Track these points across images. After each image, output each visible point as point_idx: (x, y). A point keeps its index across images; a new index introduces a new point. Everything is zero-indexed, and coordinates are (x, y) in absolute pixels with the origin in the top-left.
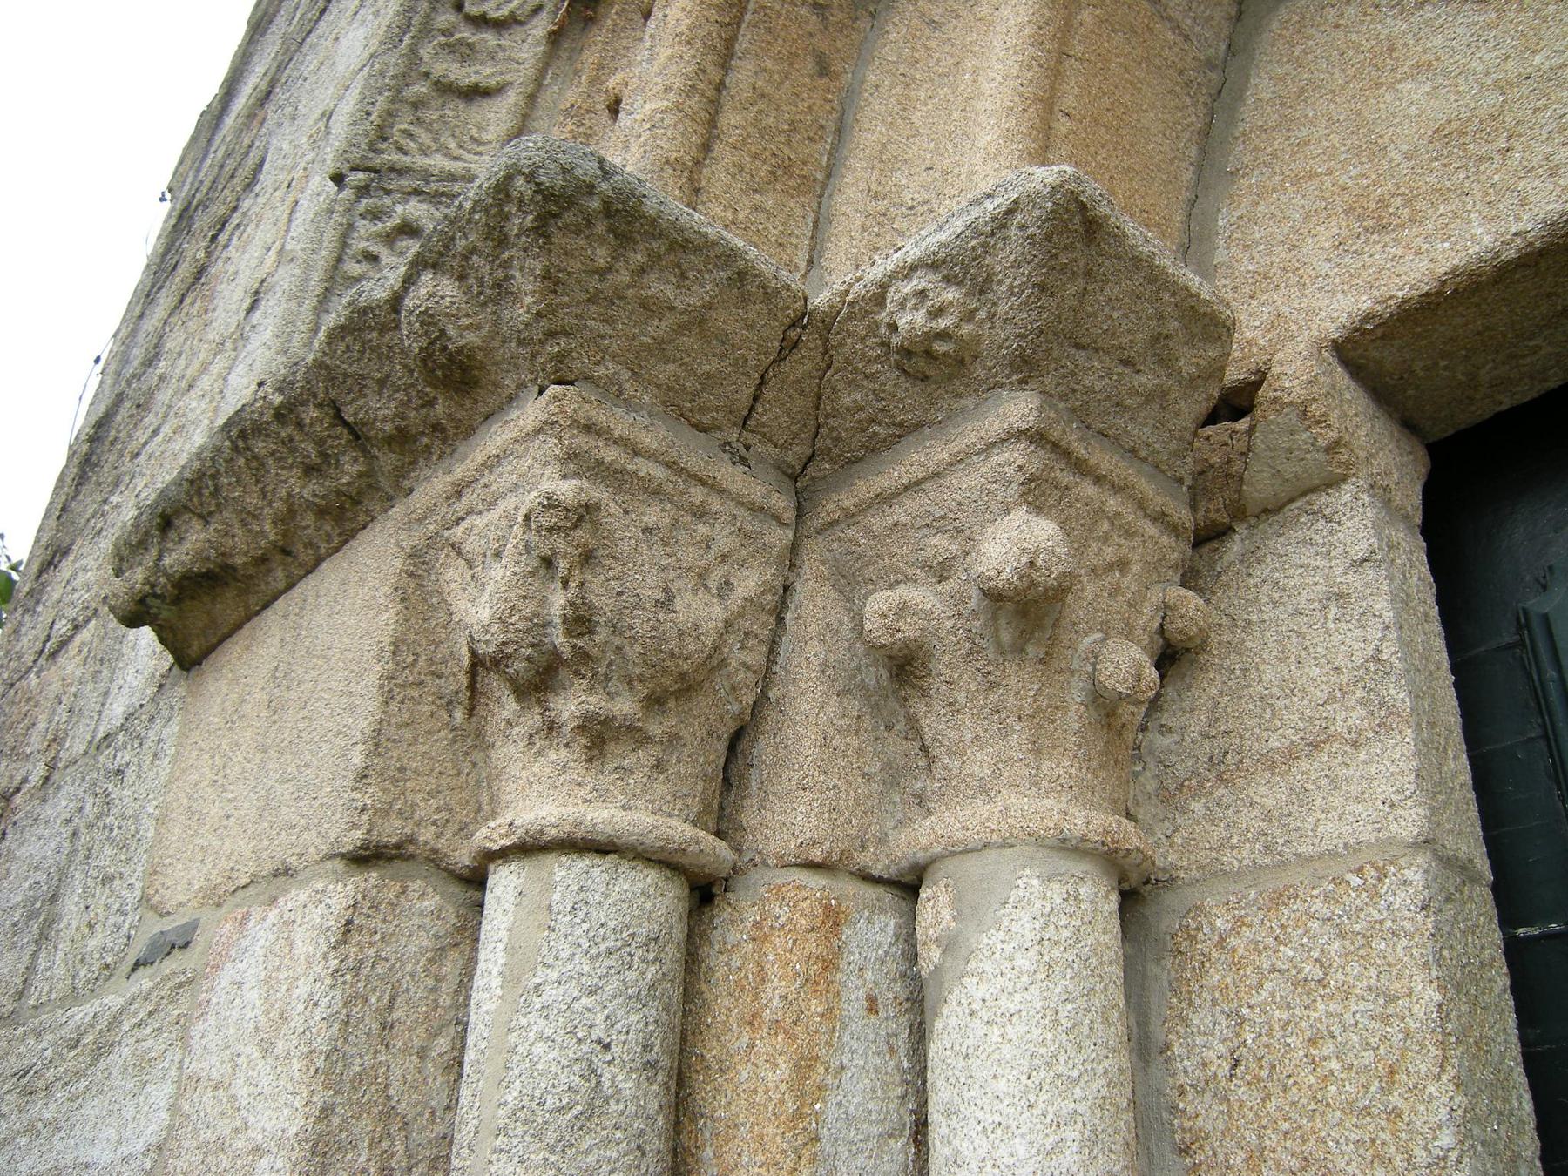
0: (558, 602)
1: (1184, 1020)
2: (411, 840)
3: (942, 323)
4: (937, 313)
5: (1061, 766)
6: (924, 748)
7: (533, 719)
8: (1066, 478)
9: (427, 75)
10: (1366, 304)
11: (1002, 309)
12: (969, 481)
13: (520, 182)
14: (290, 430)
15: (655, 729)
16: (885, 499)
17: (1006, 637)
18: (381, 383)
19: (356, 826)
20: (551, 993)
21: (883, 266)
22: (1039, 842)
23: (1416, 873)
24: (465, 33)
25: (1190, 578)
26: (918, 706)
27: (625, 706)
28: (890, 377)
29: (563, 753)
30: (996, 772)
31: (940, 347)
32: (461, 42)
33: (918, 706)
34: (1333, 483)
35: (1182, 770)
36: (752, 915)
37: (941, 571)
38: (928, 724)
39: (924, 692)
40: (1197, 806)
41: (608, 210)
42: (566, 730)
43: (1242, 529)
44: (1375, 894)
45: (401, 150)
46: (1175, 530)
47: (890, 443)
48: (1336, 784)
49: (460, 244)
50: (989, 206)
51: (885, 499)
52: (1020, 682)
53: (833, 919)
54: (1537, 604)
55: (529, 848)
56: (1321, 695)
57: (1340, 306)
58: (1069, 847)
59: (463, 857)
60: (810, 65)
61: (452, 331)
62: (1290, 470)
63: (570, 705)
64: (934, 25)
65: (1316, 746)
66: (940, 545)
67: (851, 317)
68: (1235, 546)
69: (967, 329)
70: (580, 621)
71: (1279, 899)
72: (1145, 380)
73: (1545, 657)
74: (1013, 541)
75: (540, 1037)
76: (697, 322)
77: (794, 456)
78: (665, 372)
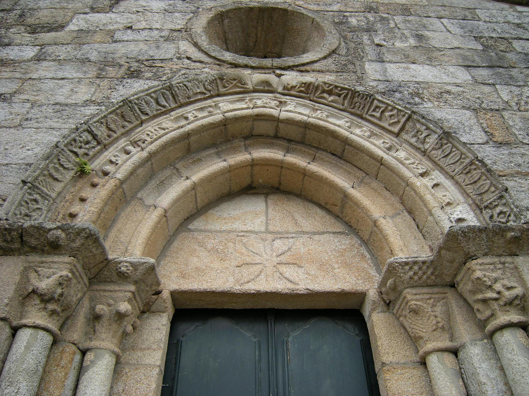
0: (59, 291)
1: (117, 384)
2: (9, 318)
3: (128, 272)
4: (128, 270)
5: (115, 341)
6: (94, 331)
7: (42, 306)
8: (133, 299)
9: (49, 171)
10: (177, 288)
11: (137, 274)
12: (121, 295)
13: (88, 230)
14: (6, 233)
15: (61, 315)
16: (105, 291)
17: (116, 319)
18: (37, 239)
19: (4, 313)
20: (34, 352)
21: (122, 259)
22: (110, 350)
23: (157, 370)
24: (57, 166)
25: (138, 318)
26: (96, 324)
27: (59, 309)
28: (115, 273)
29: (45, 313)
30: (106, 338)
31: (126, 274)
32: (57, 168)
33: (96, 324)
34: (164, 312)
35: (126, 347)
36: (61, 349)
37: (109, 305)
38: (97, 327)
39: (98, 322)
40: (128, 353)
41: (95, 239)
42: (48, 310)
43: (148, 313)
44: (151, 371)
45: (39, 184)
46: (140, 310)
47: (109, 282)
48: (150, 355)
49: (70, 231)
50: (143, 260)
51: (105, 291)
52: (115, 326)
53: (74, 353)
54: (181, 339)
55: (36, 327)
56: (152, 342)
57: (174, 286)
58: (114, 352)
59: (15, 323)
60: (115, 209)
61: (61, 241)
62: (159, 308)
63: (51, 306)
64: (136, 212)
65: (149, 349)
66: (111, 302)
67: (113, 263)
68: (146, 315)
69: (131, 274)
70: (61, 295)
71: (137, 369)
72: (148, 289)
73: (180, 347)
74: (124, 307)
75: (31, 358)
76: (94, 256)
77: (91, 277)
78: (86, 260)
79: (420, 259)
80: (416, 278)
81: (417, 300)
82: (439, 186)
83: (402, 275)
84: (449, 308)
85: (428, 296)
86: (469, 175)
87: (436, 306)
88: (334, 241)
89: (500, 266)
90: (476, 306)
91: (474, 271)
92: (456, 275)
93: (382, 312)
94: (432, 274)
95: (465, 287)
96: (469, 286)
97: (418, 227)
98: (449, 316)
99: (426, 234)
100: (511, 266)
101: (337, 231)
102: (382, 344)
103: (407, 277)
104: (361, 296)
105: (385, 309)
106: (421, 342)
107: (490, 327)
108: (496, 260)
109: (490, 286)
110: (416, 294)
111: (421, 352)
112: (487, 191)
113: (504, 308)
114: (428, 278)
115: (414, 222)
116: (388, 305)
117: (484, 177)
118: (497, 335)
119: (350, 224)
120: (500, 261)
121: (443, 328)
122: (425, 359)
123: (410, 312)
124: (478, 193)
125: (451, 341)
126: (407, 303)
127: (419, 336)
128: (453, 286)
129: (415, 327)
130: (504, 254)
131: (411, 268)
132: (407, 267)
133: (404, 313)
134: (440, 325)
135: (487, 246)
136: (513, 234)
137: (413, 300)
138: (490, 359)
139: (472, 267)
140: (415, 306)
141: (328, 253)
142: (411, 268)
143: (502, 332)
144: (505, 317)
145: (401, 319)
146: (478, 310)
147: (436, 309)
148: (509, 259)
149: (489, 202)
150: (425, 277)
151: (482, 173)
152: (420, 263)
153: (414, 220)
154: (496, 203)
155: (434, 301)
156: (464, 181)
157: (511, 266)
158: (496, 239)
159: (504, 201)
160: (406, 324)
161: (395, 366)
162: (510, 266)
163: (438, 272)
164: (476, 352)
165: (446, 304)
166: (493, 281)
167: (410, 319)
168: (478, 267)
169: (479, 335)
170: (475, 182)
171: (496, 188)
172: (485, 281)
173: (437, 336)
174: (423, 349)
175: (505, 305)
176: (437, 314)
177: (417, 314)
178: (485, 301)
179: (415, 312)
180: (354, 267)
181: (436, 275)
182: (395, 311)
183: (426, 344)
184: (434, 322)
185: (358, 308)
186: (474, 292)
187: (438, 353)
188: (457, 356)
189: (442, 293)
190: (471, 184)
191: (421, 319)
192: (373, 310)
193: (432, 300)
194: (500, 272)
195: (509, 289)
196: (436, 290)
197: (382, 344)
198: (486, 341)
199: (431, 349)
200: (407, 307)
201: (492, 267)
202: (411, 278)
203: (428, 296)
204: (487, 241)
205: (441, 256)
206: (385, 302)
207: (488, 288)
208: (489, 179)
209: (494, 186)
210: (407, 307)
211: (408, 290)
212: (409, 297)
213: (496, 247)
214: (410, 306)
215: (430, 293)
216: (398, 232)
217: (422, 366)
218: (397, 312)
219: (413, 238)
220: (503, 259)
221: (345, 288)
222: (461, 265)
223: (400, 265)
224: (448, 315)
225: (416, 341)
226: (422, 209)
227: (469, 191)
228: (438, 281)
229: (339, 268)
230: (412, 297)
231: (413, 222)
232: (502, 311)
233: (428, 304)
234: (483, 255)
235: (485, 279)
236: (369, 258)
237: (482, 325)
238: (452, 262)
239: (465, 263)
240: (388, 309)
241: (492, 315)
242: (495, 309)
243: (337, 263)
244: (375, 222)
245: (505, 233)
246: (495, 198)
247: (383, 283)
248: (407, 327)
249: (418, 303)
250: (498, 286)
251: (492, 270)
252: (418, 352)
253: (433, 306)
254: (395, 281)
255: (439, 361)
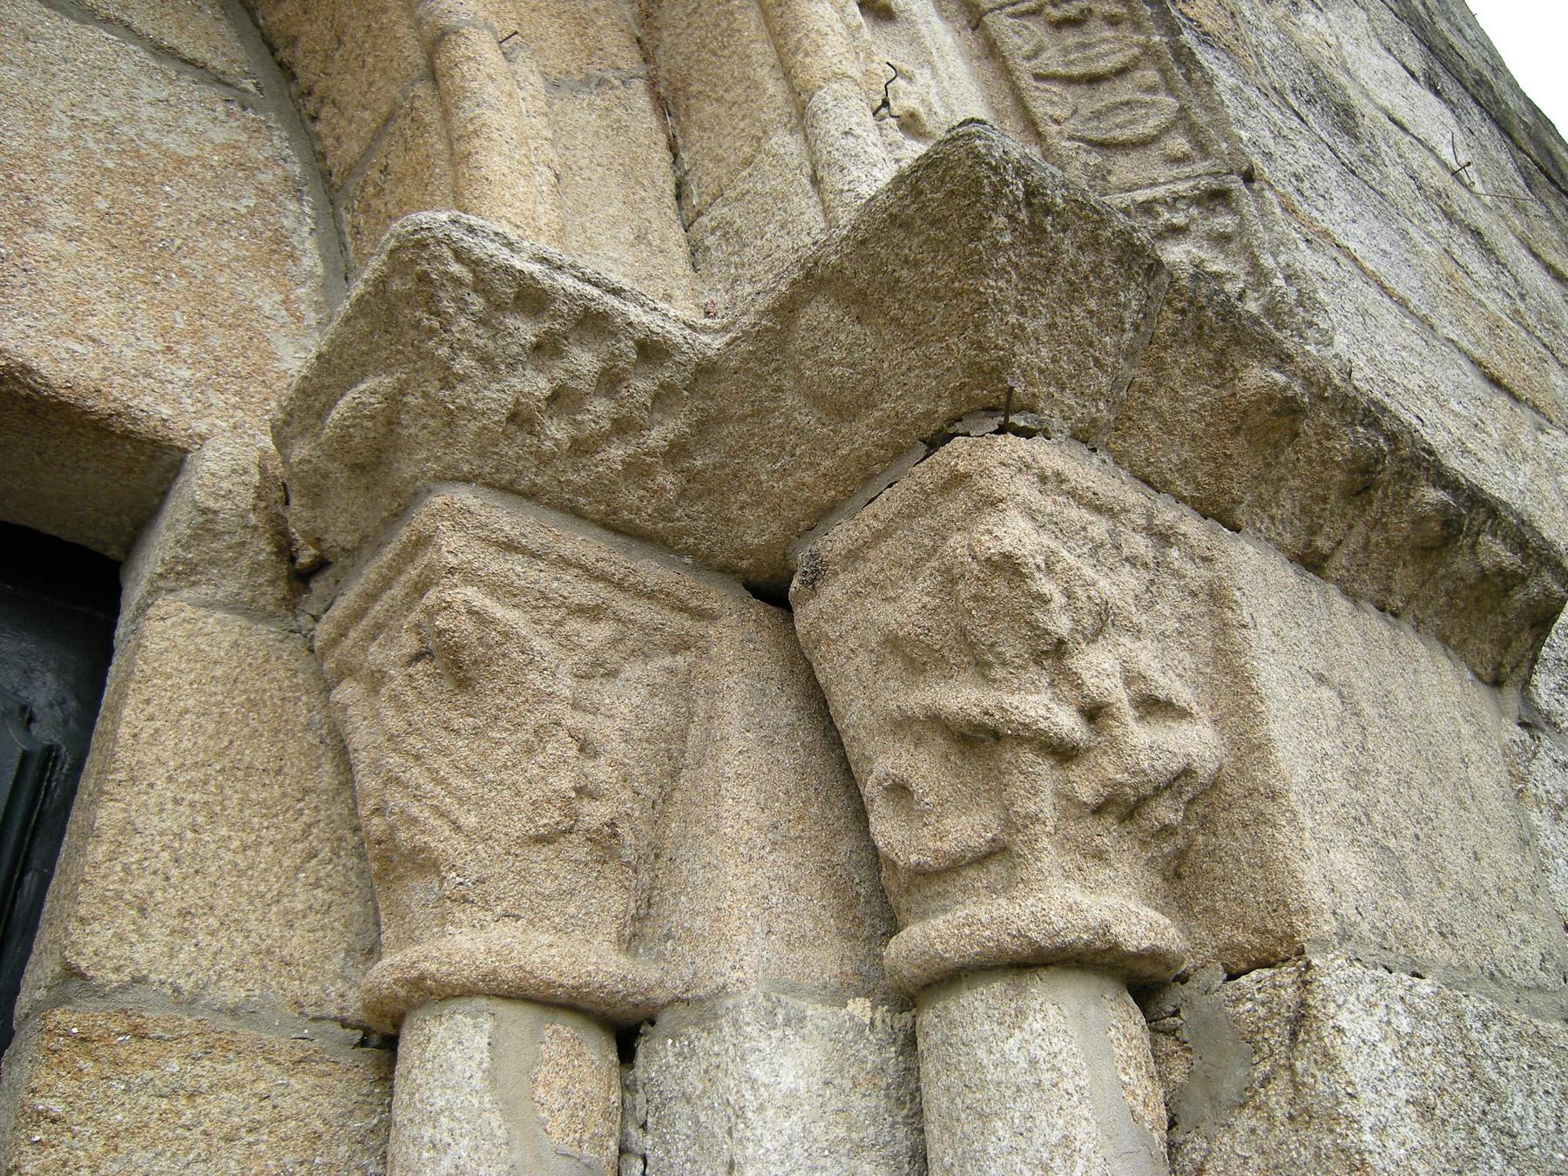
79: (634, 313)
80: (557, 431)
81: (500, 589)
82: (890, 28)
83: (464, 363)
84: (691, 714)
85: (585, 592)
86: (1071, 38)
87: (612, 674)
88: (134, 83)
89: (1140, 545)
90: (886, 760)
91: (993, 503)
92: (824, 514)
93: (232, 606)
94: (676, 452)
95: (854, 613)
96: (909, 606)
97: (680, 195)
98: (674, 775)
99: (710, 240)
100: (1196, 574)
101: (188, 52)
102: (129, 828)
103: (495, 396)
104: (155, 463)
105: (271, 596)
106: (417, 892)
107: (935, 933)
108: (1132, 496)
109: (1059, 649)
110: (509, 546)
111: (389, 969)
112: (1144, 143)
113: (1090, 826)
114: (636, 470)
115: (668, 157)
116: (301, 574)
117: (1151, 75)
118: (977, 1006)
119: (284, 55)
120: (1150, 517)
121: (605, 842)
122: (398, 1021)
123: (418, 657)
124: (1093, 135)
125: (630, 942)
126: (420, 588)
127: (417, 850)
128: (772, 592)
129: (416, 774)
130: (1180, 485)
131: (546, 349)
132: (526, 330)
133: (376, 654)
134: (596, 813)
135: (1116, 385)
136: (1280, 378)
137: (470, 576)
138: (858, 1149)
139: (985, 472)
140: (467, 625)
141: (46, 122)
142: (546, 349)
143: (1021, 992)
144: (1075, 894)
145: (347, 692)
146: (899, 790)
147: (604, 692)
148: (1192, 527)
149: (1141, 196)
150: (616, 453)
151: (1146, 48)
152: (627, 346)
153: (673, 148)
154: (1179, 219)
155: (614, 643)
156: (1035, 54)
157: (1196, 574)
158: (1180, 360)
159: (1224, 222)
160: (361, 737)
161: (155, 1019)
162: (1190, 569)
163: (714, 458)
164: (788, 1080)
165: (683, 688)
166: (1088, 621)
167: (402, 707)
168: (1024, 488)
169: (828, 960)
170: (1093, 80)
171: (1203, 149)
172: (1044, 600)
173: (549, 886)
174: (413, 953)
175: (1098, 811)
176: (603, 729)
177: (463, 684)
178: (977, 741)
179: (456, 665)
180: (183, 273)
181: (692, 477)
182: (323, 631)
183: (443, 919)
184: (564, 783)
185: (113, 552)
186: (910, 656)
187: (506, 1010)
188: (627, 1055)
189: (683, 608)
190: (1069, 80)
191: (477, 732)
192: (183, 573)
193: (602, 631)
194: (1131, 580)
195: (1153, 706)
196: (652, 570)
197: (129, 828)
198: (859, 1008)
199: (468, 974)
200: (414, 617)
201: (1099, 528)
202: (520, 418)
203: (585, 592)
204: (1130, 354)
205: (781, 347)
206: (285, 550)
207: (1038, 658)
208: (1171, 91)
209: (1192, 130)
210: (414, 617)
211: (465, 496)
212: (452, 546)
213: (1158, 414)
214: (431, 613)
215: (603, 578)
216: (552, 154)
217: (365, 1058)
218: (334, 643)
219: (626, 233)
220: (1168, 513)
221: (44, 365)
222: (899, 452)
223: (482, 286)
224: (673, 762)
225: (381, 876)
226: (756, 85)
227: (1040, 109)
228: (693, 517)
229: (71, 234)
230: (477, 553)
231: (661, 156)
232: (1063, 842)
233: (569, 644)
234: (1074, 436)
235: (1047, 587)
236: (311, 275)
237: (878, 895)
238: (840, 407)
239: (935, 442)
240: (291, 604)
241: (996, 852)
242: (1035, 819)
243: (83, 203)
244: (437, 41)
245: (1235, 353)
246: (1181, 187)
247: (306, 406)
248: (362, 762)
249: (498, 611)
250: (1099, 667)
251: (1097, 547)
252: (372, 952)
253: (599, 669)
254: (395, 399)
255: (492, 1076)
